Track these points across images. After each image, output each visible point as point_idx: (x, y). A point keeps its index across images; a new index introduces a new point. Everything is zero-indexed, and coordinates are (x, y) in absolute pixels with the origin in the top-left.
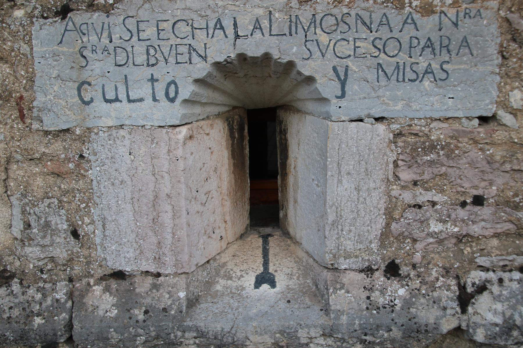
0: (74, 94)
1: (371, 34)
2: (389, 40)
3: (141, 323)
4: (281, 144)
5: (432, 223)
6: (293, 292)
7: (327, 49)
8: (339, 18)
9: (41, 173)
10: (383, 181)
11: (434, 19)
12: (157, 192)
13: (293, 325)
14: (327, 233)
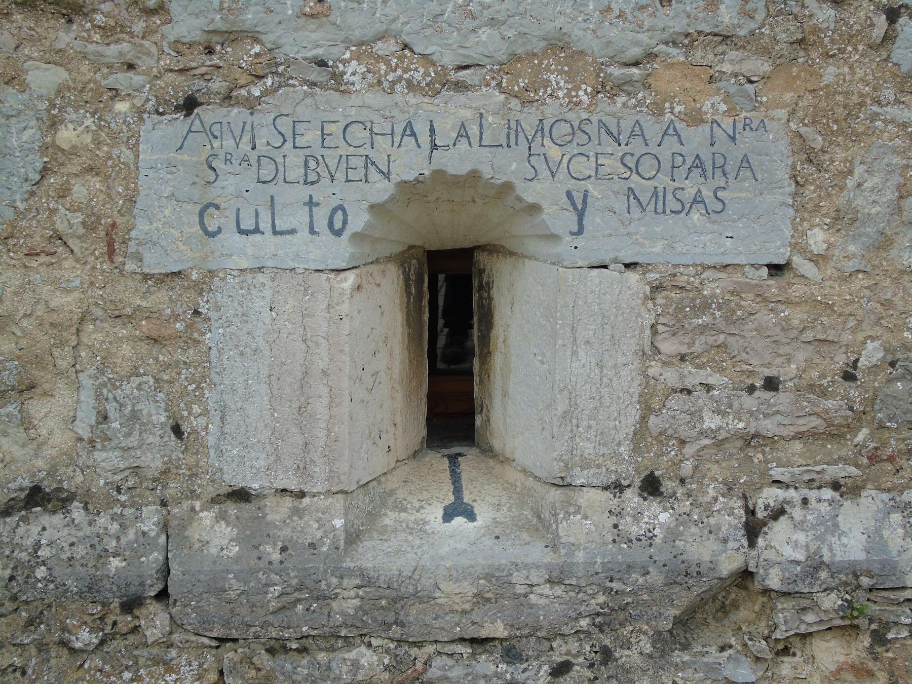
0: (194, 221)
1: (619, 148)
2: (644, 157)
3: (276, 565)
4: (481, 306)
5: (706, 415)
6: (503, 526)
7: (558, 167)
8: (576, 124)
9: (128, 339)
10: (637, 354)
11: (703, 131)
12: (309, 366)
13: (506, 565)
14: (555, 430)
